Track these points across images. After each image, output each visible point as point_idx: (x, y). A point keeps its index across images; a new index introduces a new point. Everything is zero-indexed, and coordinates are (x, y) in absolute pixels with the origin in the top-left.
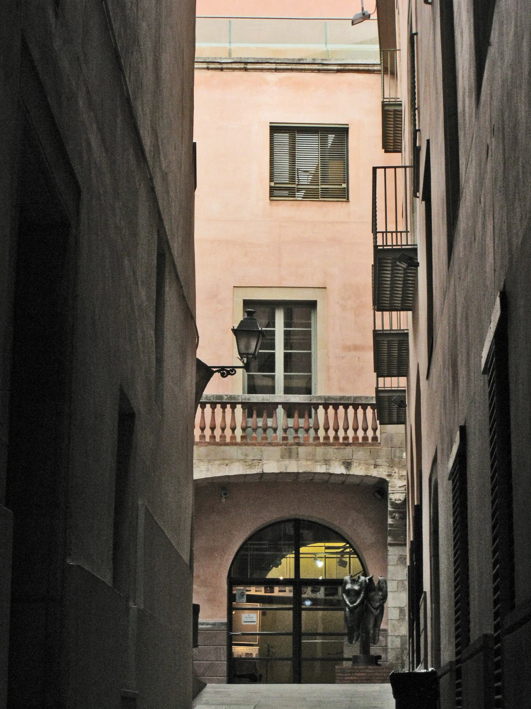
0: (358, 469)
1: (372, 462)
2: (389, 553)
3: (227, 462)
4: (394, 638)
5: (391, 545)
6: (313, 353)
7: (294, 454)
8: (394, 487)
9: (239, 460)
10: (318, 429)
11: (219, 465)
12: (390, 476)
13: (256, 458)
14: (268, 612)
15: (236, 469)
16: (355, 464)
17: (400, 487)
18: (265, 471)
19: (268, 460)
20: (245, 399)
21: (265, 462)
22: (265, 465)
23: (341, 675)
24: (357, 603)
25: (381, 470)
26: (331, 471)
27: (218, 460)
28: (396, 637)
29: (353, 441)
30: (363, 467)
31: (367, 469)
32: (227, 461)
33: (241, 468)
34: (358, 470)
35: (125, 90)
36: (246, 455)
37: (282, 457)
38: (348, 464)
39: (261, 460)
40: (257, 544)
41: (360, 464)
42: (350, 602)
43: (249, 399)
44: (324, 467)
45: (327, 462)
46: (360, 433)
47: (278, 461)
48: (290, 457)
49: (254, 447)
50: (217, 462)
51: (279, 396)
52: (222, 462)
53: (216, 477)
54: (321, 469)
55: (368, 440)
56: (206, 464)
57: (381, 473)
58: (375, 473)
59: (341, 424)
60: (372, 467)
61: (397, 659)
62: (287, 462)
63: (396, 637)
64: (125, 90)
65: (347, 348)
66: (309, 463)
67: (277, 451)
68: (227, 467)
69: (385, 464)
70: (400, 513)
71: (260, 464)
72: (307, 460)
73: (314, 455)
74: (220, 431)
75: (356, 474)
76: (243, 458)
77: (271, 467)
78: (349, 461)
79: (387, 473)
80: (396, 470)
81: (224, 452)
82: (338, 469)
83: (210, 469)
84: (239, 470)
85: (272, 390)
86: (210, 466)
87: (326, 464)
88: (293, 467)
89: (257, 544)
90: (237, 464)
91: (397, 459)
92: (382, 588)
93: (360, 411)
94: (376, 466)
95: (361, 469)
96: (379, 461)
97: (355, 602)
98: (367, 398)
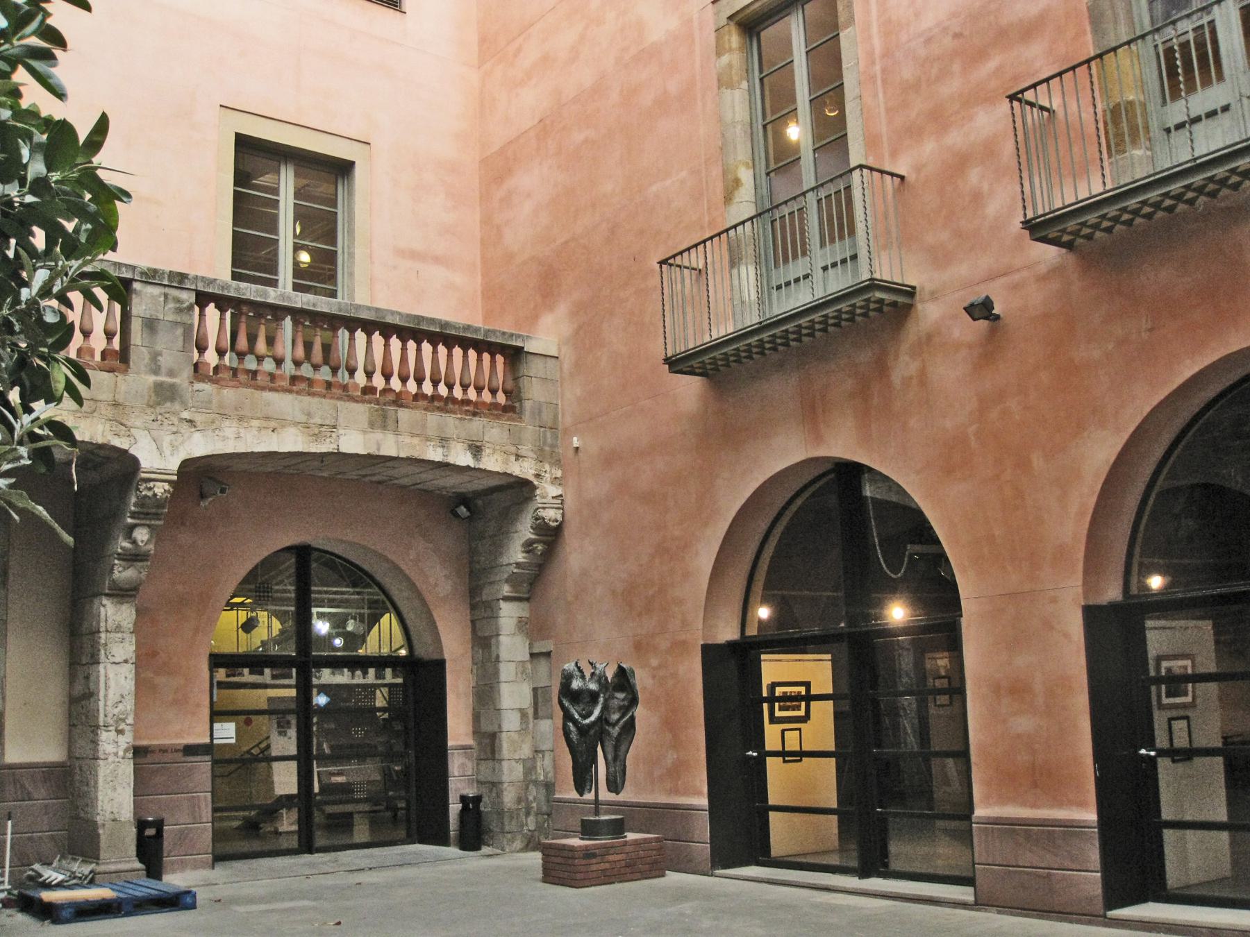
0: (493, 459)
1: (513, 449)
2: (502, 613)
3: (273, 424)
4: (513, 763)
5: (506, 599)
6: (340, 252)
7: (390, 422)
11: (260, 429)
12: (538, 476)
13: (327, 422)
14: (253, 717)
15: (291, 441)
16: (488, 451)
18: (343, 449)
19: (346, 427)
20: (308, 304)
22: (342, 438)
23: (584, 862)
24: (592, 718)
26: (451, 460)
28: (517, 761)
30: (499, 457)
31: (506, 462)
32: (275, 423)
33: (300, 438)
34: (492, 462)
37: (372, 425)
38: (476, 450)
39: (334, 427)
40: (335, 593)
41: (494, 450)
42: (580, 715)
43: (314, 305)
44: (440, 450)
45: (444, 441)
47: (364, 432)
48: (384, 427)
50: (255, 423)
52: (265, 424)
53: (252, 453)
54: (435, 455)
56: (234, 425)
57: (524, 469)
60: (513, 458)
61: (519, 800)
62: (378, 435)
63: (517, 761)
65: (401, 253)
66: (416, 441)
67: (361, 411)
68: (275, 435)
69: (531, 454)
70: (544, 543)
71: (334, 435)
72: (413, 435)
73: (424, 426)
75: (489, 468)
76: (303, 419)
77: (353, 442)
79: (533, 472)
80: (547, 467)
81: (269, 404)
82: (463, 458)
86: (242, 430)
88: (389, 446)
89: (335, 593)
91: (547, 448)
92: (439, 666)
94: (518, 457)
96: (524, 450)
97: (590, 714)
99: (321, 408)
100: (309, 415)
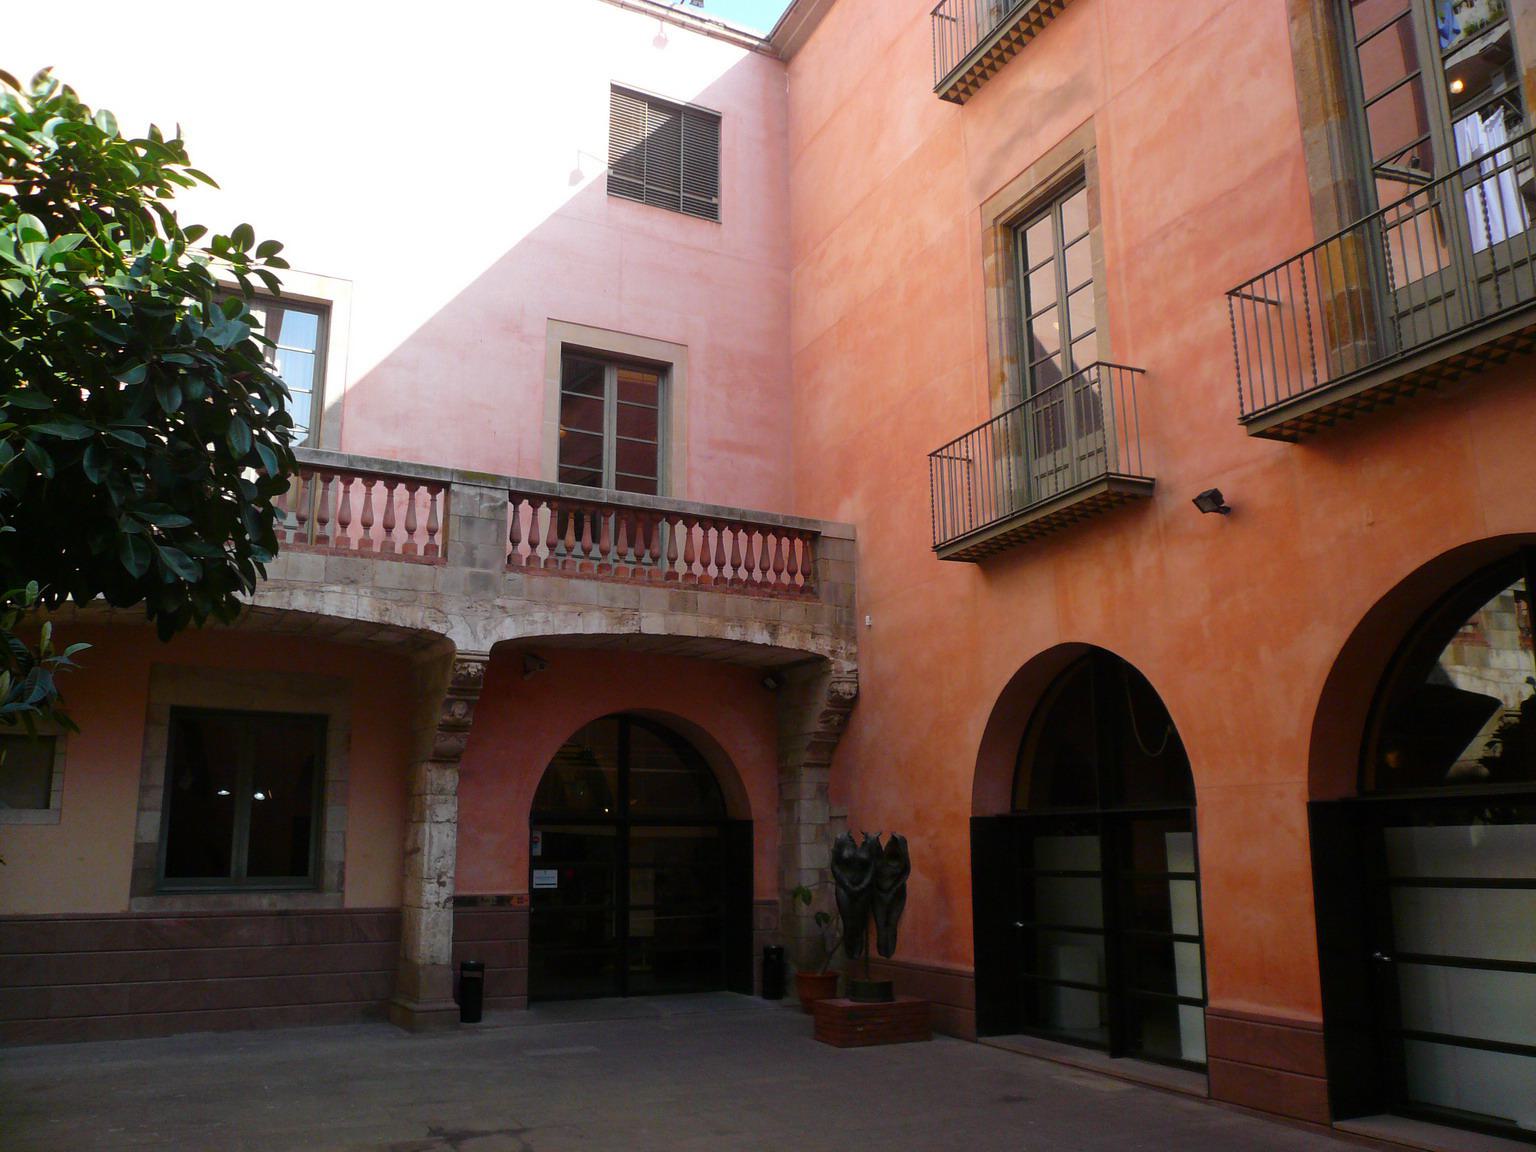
0: (789, 637)
3: (579, 609)
5: (807, 765)
8: (839, 673)
9: (600, 608)
10: (676, 559)
12: (833, 652)
15: (595, 624)
17: (849, 672)
18: (645, 630)
21: (644, 614)
25: (821, 641)
27: (566, 604)
29: (360, 547)
31: (802, 639)
32: (582, 608)
33: (604, 621)
34: (788, 641)
35: (1362, 201)
36: (613, 599)
38: (774, 630)
39: (637, 610)
45: (742, 622)
46: (697, 568)
47: (665, 614)
48: (684, 610)
49: (626, 586)
50: (562, 608)
51: (608, 492)
54: (733, 634)
55: (677, 578)
58: (812, 646)
59: (378, 519)
64: (1362, 201)
66: (714, 621)
67: (661, 595)
68: (580, 620)
71: (636, 617)
74: (383, 531)
76: (607, 603)
77: (653, 624)
78: (775, 623)
79: (829, 648)
80: (843, 644)
82: (760, 637)
83: (550, 619)
84: (600, 625)
85: (595, 480)
86: (550, 615)
87: (741, 626)
88: (689, 625)
90: (597, 614)
91: (843, 626)
93: (713, 532)
94: (814, 635)
95: (793, 638)
96: (820, 628)
98: (802, 520)
99: (623, 594)
100: (613, 599)
